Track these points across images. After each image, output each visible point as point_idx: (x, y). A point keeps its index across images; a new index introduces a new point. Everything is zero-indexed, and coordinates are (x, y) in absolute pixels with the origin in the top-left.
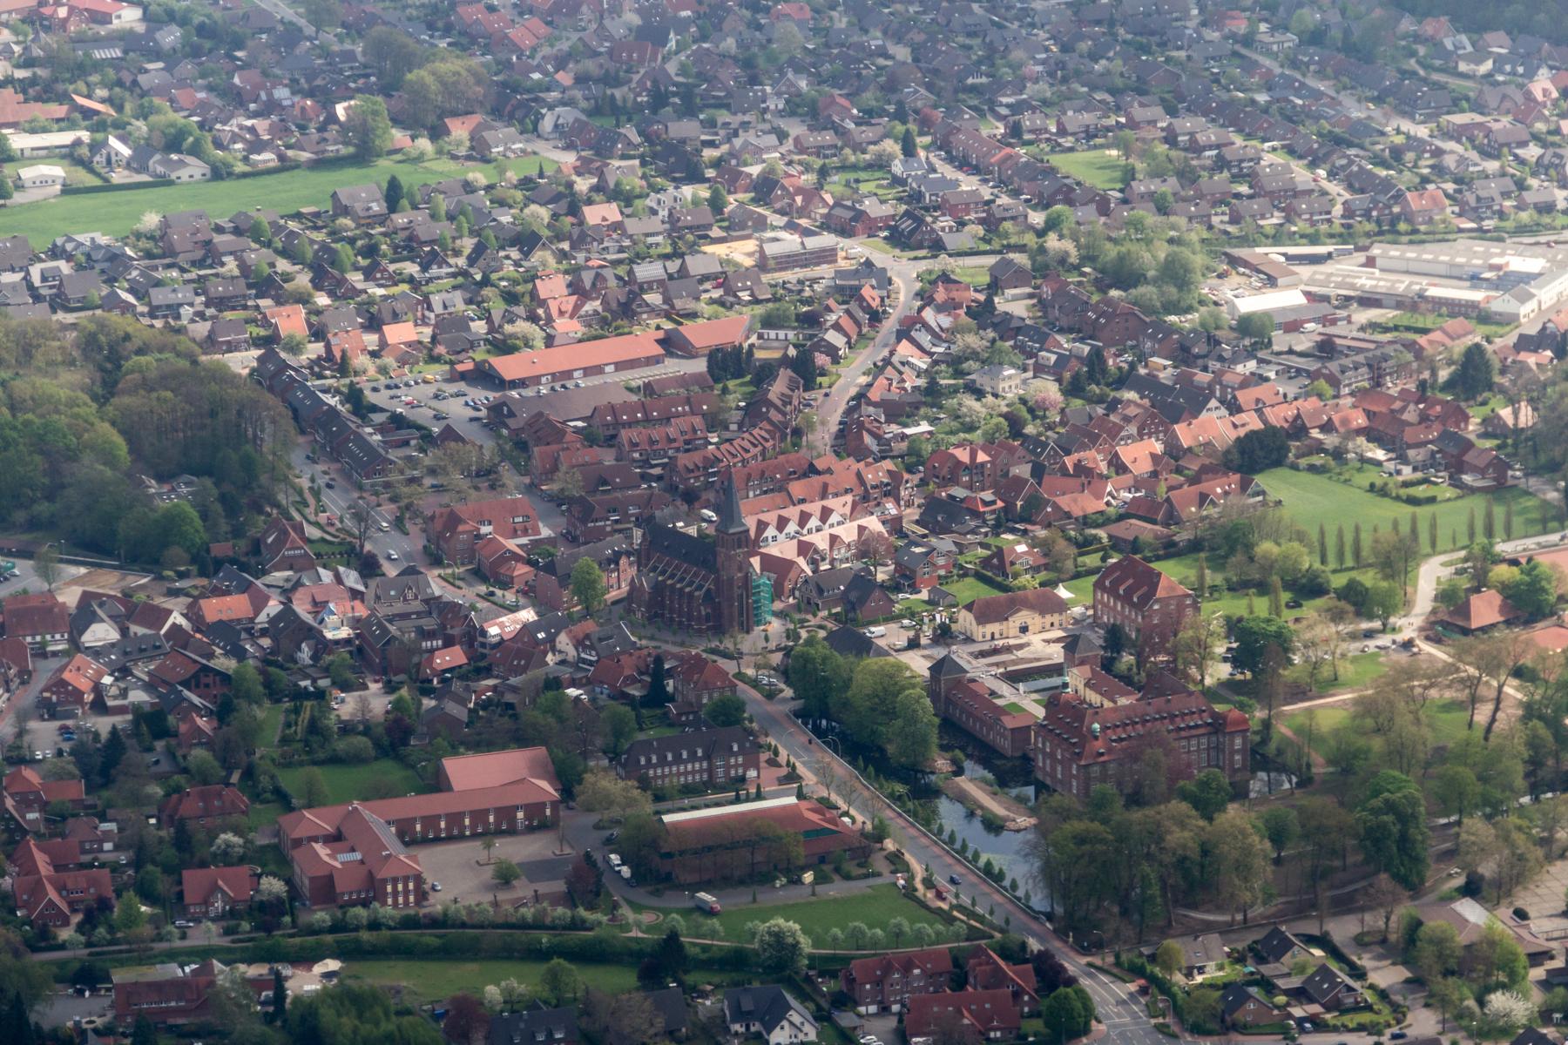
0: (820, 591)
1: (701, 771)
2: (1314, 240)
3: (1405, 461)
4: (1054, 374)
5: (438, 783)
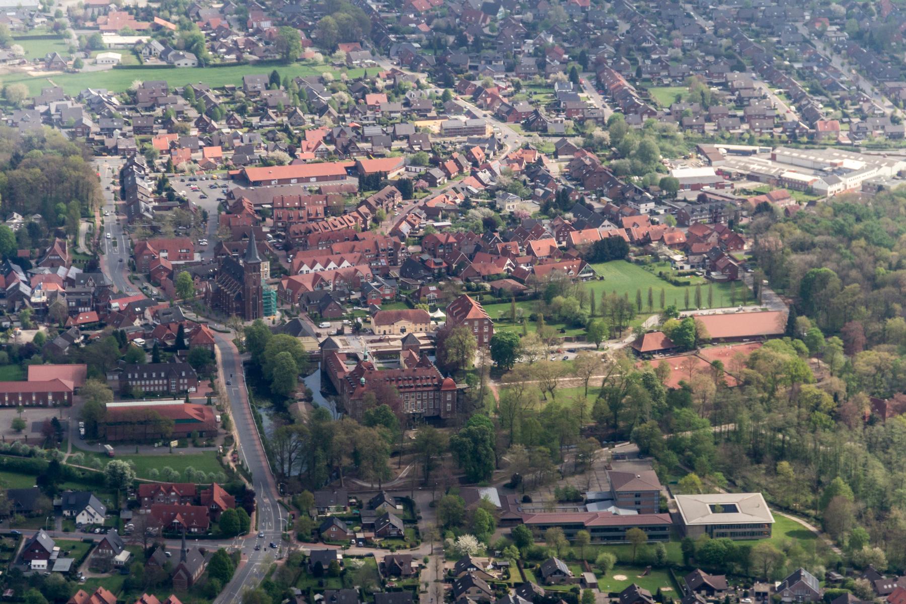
1: (163, 385)
2: (751, 142)
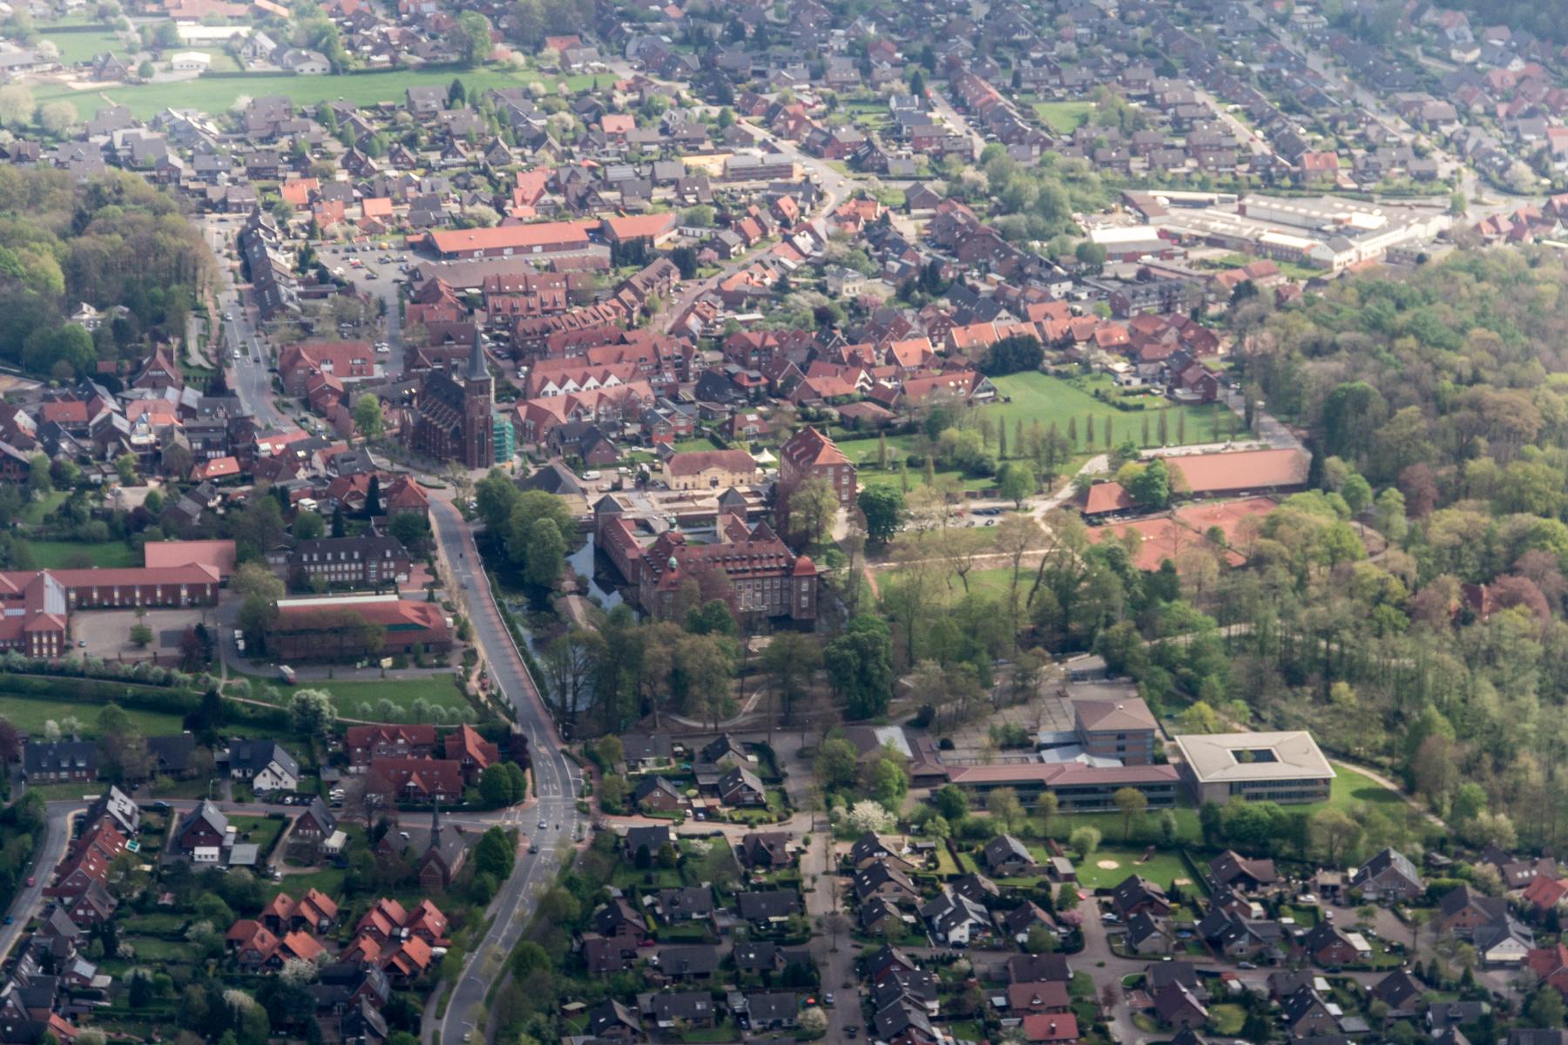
0: (562, 438)
2: (1204, 186)
3: (1136, 374)
5: (140, 562)
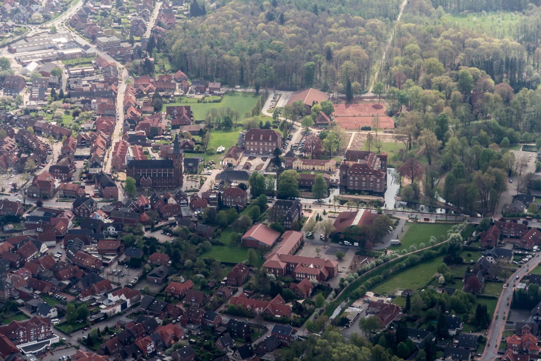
4: (41, 100)
